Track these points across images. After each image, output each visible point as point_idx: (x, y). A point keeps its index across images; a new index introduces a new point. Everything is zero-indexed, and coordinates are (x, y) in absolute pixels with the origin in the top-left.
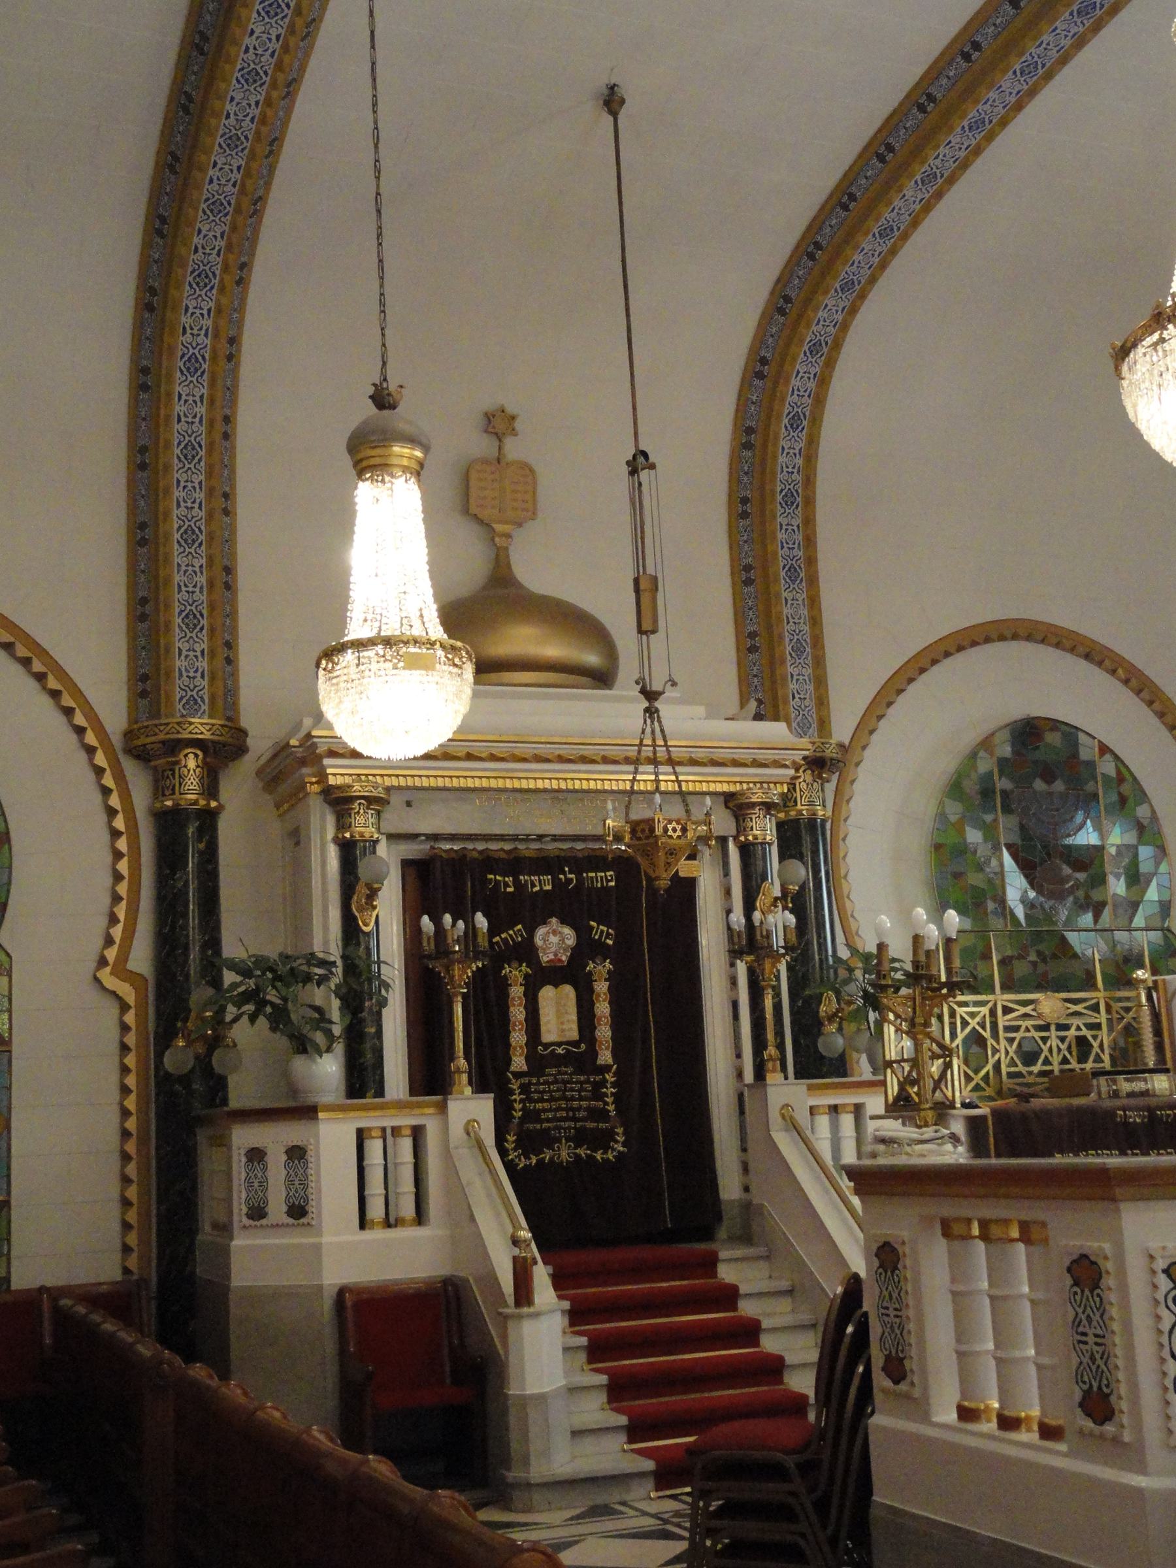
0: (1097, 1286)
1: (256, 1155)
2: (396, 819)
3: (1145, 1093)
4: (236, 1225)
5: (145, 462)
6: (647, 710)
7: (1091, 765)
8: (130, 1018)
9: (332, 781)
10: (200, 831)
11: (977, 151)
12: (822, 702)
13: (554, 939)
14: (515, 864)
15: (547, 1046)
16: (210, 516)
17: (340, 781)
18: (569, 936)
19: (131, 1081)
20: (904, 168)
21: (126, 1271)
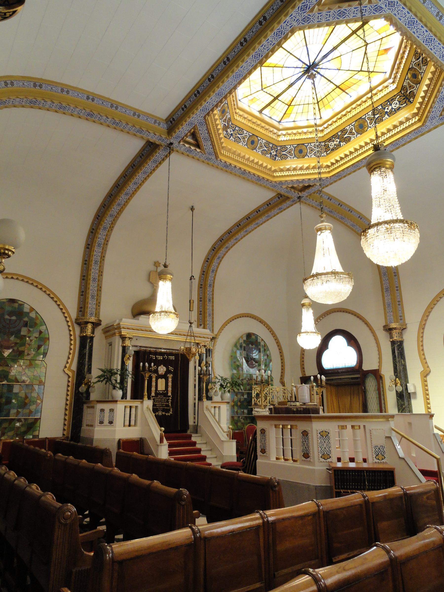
0: (307, 435)
1: (102, 410)
2: (134, 342)
3: (295, 406)
4: (96, 425)
5: (86, 263)
6: (190, 326)
7: (260, 343)
8: (70, 380)
9: (122, 333)
10: (90, 342)
11: (256, 228)
12: (213, 326)
13: (162, 369)
14: (156, 353)
15: (159, 391)
16: (99, 276)
17: (124, 333)
18: (165, 369)
19: (69, 393)
20: (242, 228)
21: (64, 435)
